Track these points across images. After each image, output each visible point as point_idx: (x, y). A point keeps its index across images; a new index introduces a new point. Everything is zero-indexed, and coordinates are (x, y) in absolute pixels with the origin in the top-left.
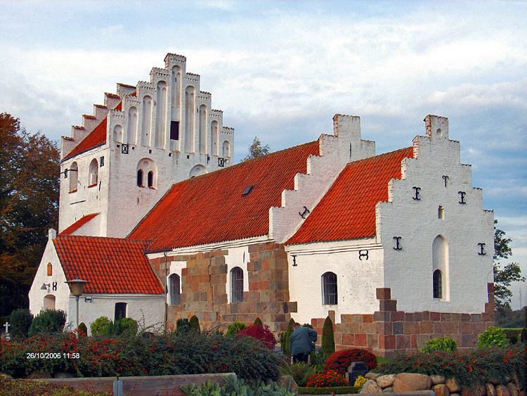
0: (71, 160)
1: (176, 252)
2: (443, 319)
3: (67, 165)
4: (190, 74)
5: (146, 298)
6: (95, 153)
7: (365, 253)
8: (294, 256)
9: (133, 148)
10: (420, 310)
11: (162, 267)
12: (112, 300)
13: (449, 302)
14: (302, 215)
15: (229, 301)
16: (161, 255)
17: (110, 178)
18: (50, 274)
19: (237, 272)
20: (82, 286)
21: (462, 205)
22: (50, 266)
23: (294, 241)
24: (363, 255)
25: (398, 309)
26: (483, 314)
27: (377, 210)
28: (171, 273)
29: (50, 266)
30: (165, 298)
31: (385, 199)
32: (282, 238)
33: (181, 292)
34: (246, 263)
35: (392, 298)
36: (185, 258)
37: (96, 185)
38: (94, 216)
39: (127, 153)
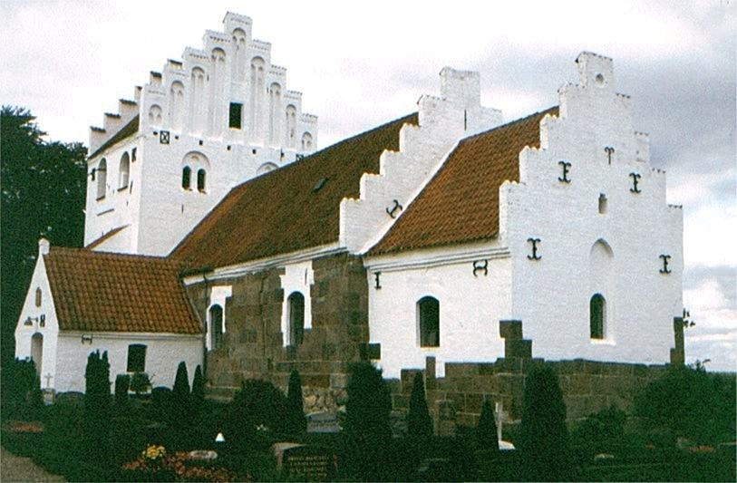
0: (99, 158)
1: (220, 273)
2: (606, 371)
3: (94, 165)
4: (258, 41)
5: (176, 339)
6: (126, 146)
7: (483, 264)
8: (378, 274)
9: (177, 138)
10: (570, 356)
11: (201, 295)
12: (123, 342)
13: (607, 349)
14: (391, 214)
15: (286, 342)
16: (200, 279)
17: (142, 182)
18: (38, 304)
19: (297, 298)
20: (73, 321)
21: (534, 262)
22: (39, 291)
23: (376, 252)
24: (480, 268)
25: (535, 355)
26: (667, 365)
27: (503, 196)
28: (212, 304)
29: (39, 291)
30: (204, 340)
31: (515, 177)
32: (359, 247)
33: (224, 330)
34: (308, 285)
35: (526, 336)
36: (228, 281)
37: (126, 187)
38: (126, 226)
39: (168, 142)
